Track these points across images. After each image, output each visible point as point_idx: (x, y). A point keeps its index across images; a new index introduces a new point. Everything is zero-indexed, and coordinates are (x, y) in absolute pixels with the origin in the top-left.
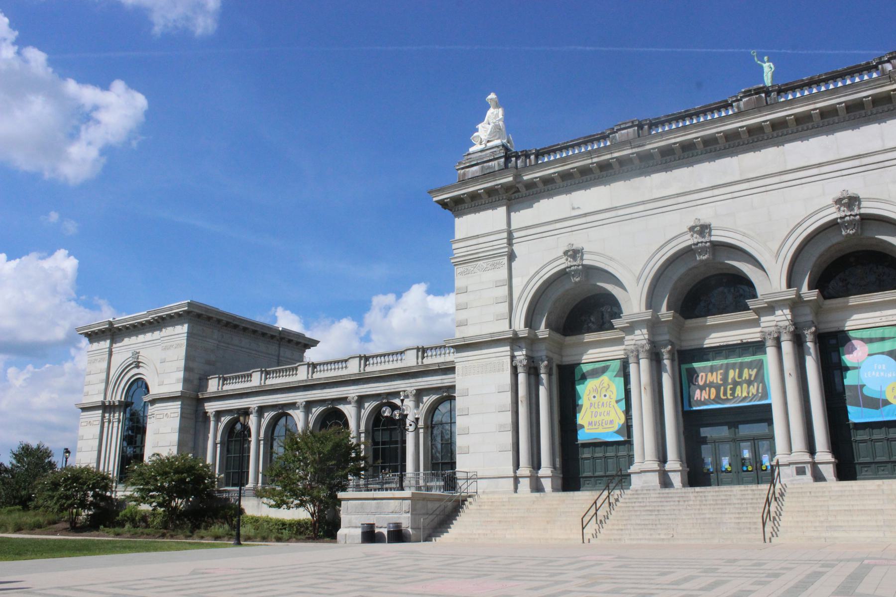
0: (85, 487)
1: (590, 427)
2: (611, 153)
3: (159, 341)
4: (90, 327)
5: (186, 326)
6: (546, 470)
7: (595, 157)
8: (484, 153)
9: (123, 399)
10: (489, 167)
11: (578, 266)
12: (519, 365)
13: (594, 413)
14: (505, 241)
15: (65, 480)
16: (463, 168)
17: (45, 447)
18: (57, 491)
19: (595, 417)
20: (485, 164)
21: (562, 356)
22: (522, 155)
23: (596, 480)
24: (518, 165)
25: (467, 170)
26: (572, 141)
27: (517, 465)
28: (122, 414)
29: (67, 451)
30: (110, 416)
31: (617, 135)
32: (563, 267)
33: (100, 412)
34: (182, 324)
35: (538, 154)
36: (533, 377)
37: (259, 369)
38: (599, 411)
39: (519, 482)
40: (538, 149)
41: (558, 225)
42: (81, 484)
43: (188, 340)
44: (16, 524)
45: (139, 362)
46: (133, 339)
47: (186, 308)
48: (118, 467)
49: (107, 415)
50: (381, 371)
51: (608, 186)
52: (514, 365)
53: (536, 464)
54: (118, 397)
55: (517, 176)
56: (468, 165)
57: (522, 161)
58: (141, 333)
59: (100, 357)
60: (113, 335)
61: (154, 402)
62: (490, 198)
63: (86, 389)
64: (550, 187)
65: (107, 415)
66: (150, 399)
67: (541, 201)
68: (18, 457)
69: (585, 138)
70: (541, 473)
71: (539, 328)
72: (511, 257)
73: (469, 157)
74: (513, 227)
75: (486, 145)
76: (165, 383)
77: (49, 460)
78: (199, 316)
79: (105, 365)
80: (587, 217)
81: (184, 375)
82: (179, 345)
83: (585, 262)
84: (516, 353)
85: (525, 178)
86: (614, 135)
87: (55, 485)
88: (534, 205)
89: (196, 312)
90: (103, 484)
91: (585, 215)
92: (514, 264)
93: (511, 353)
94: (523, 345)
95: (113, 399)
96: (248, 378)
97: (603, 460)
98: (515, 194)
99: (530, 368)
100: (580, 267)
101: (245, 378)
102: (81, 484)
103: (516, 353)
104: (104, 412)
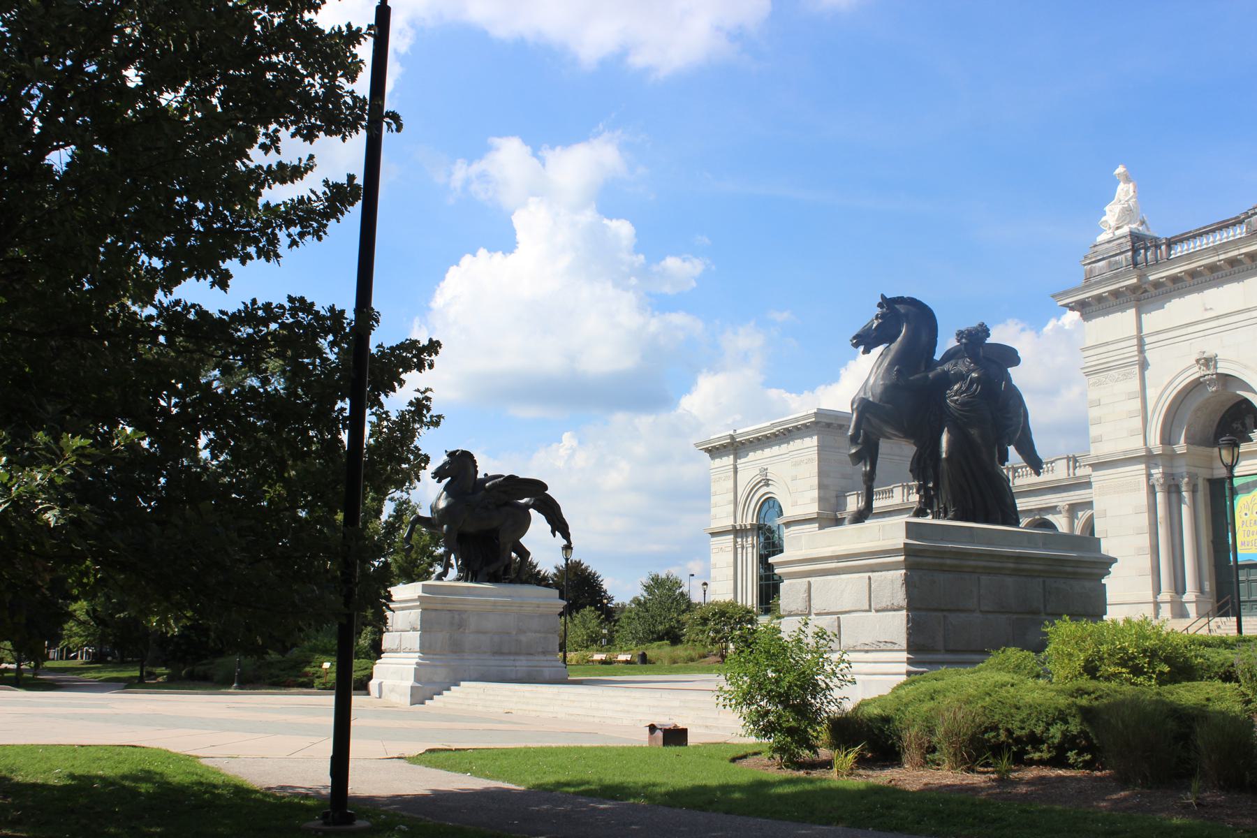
0: (732, 621)
1: (1243, 547)
2: (1239, 249)
3: (787, 455)
4: (709, 442)
5: (815, 438)
6: (1190, 595)
7: (1221, 254)
8: (1111, 245)
9: (755, 522)
10: (1116, 263)
11: (1212, 375)
12: (1156, 483)
13: (1246, 532)
14: (1136, 348)
15: (714, 615)
16: (1089, 264)
17: (675, 576)
18: (707, 625)
19: (1248, 536)
20: (1112, 259)
21: (1212, 469)
22: (1152, 246)
23: (1253, 605)
24: (1148, 258)
25: (1094, 265)
26: (1205, 228)
27: (1157, 590)
28: (755, 538)
29: (705, 584)
30: (742, 541)
31: (1252, 219)
32: (1197, 376)
33: (732, 536)
34: (811, 436)
35: (1170, 243)
36: (1174, 496)
37: (900, 484)
38: (1251, 529)
39: (1160, 608)
40: (1169, 237)
41: (1190, 329)
42: (728, 618)
43: (819, 454)
44: (671, 658)
45: (768, 480)
46: (758, 454)
47: (813, 419)
48: (757, 597)
49: (739, 540)
50: (1029, 485)
51: (1241, 283)
52: (1151, 484)
53: (1179, 588)
54: (749, 520)
55: (1142, 277)
56: (1093, 260)
57: (1152, 253)
58: (767, 447)
59: (725, 475)
60: (736, 450)
61: (788, 524)
62: (1118, 300)
63: (713, 511)
64: (1179, 285)
65: (739, 540)
66: (785, 521)
67: (1173, 301)
68: (648, 588)
69: (1218, 223)
70: (1186, 598)
71: (1178, 443)
72: (1144, 365)
73: (1096, 249)
74: (1144, 332)
75: (1114, 233)
76: (798, 504)
77: (680, 591)
78: (829, 425)
79: (731, 484)
80: (1220, 320)
81: (819, 493)
82: (810, 460)
83: (1219, 371)
84: (1153, 471)
85: (1151, 278)
86: (1249, 220)
87: (705, 621)
88: (1165, 306)
89: (825, 422)
90: (748, 617)
91: (1217, 317)
92: (1147, 373)
93: (1146, 471)
94: (1160, 462)
95: (744, 522)
96: (889, 493)
97: (1246, 584)
98: (1144, 294)
99: (1170, 486)
100: (1214, 376)
101: (886, 494)
102: (728, 618)
103: (1153, 471)
104: (736, 537)
